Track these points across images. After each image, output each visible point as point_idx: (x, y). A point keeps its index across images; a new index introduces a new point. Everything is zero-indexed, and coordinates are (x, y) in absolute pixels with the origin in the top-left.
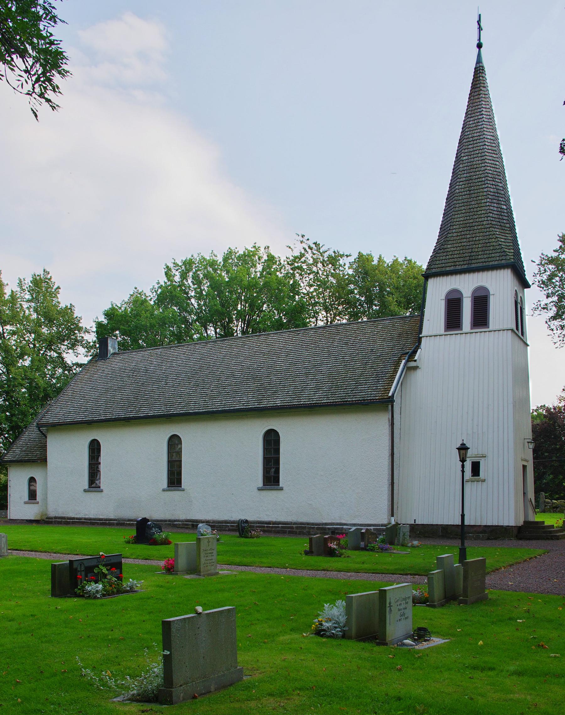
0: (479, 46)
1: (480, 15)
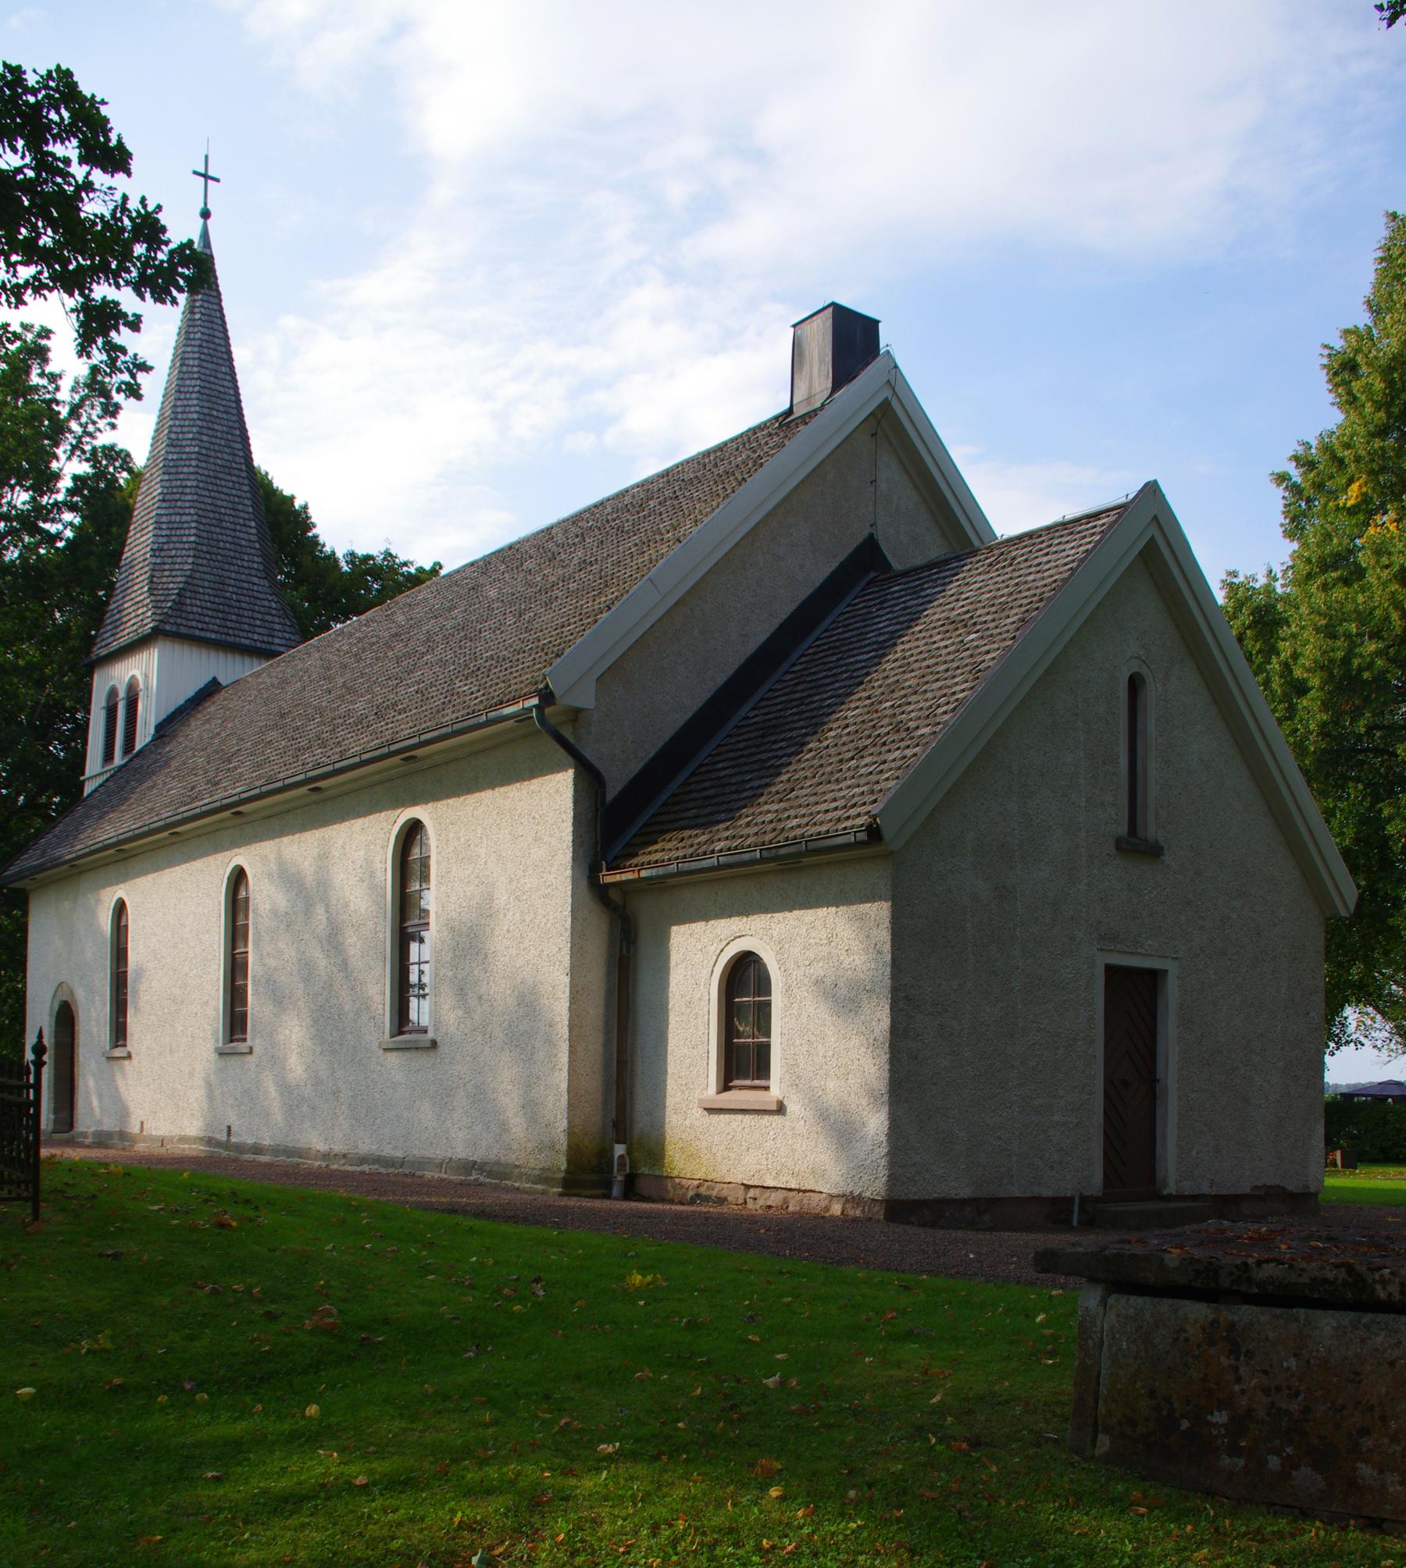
0: (206, 214)
1: (207, 157)
